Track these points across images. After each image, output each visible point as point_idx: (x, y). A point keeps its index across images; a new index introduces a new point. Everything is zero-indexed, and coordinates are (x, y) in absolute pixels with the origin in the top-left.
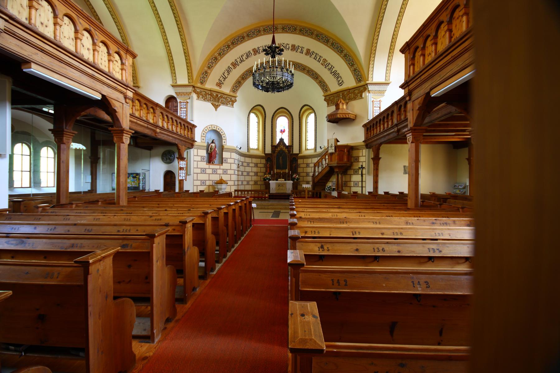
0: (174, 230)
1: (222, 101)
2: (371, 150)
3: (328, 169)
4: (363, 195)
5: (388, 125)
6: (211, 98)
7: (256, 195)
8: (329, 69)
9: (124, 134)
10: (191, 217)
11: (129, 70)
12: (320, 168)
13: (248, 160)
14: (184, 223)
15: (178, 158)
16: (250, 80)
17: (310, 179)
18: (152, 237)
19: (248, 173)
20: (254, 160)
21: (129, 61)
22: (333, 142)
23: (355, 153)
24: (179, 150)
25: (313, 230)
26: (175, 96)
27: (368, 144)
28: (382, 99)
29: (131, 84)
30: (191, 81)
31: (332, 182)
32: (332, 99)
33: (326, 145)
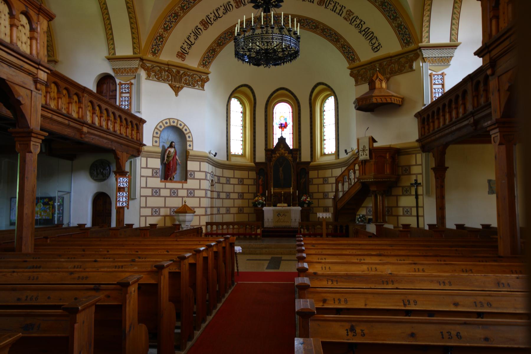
0: (108, 296)
1: (186, 80)
2: (431, 154)
3: (358, 187)
4: (419, 230)
5: (457, 114)
6: (168, 77)
7: (242, 231)
8: (357, 26)
9: (32, 139)
10: (135, 275)
11: (42, 39)
12: (346, 185)
13: (228, 173)
14: (125, 285)
15: (116, 173)
16: (230, 47)
17: (329, 203)
18: (73, 312)
19: (228, 194)
20: (238, 174)
21: (42, 25)
22: (366, 143)
23: (403, 160)
24: (117, 159)
25: (337, 296)
26: (113, 74)
27: (425, 144)
28: (445, 71)
29: (44, 58)
30: (137, 50)
31: (367, 207)
32: (361, 73)
33: (355, 147)
